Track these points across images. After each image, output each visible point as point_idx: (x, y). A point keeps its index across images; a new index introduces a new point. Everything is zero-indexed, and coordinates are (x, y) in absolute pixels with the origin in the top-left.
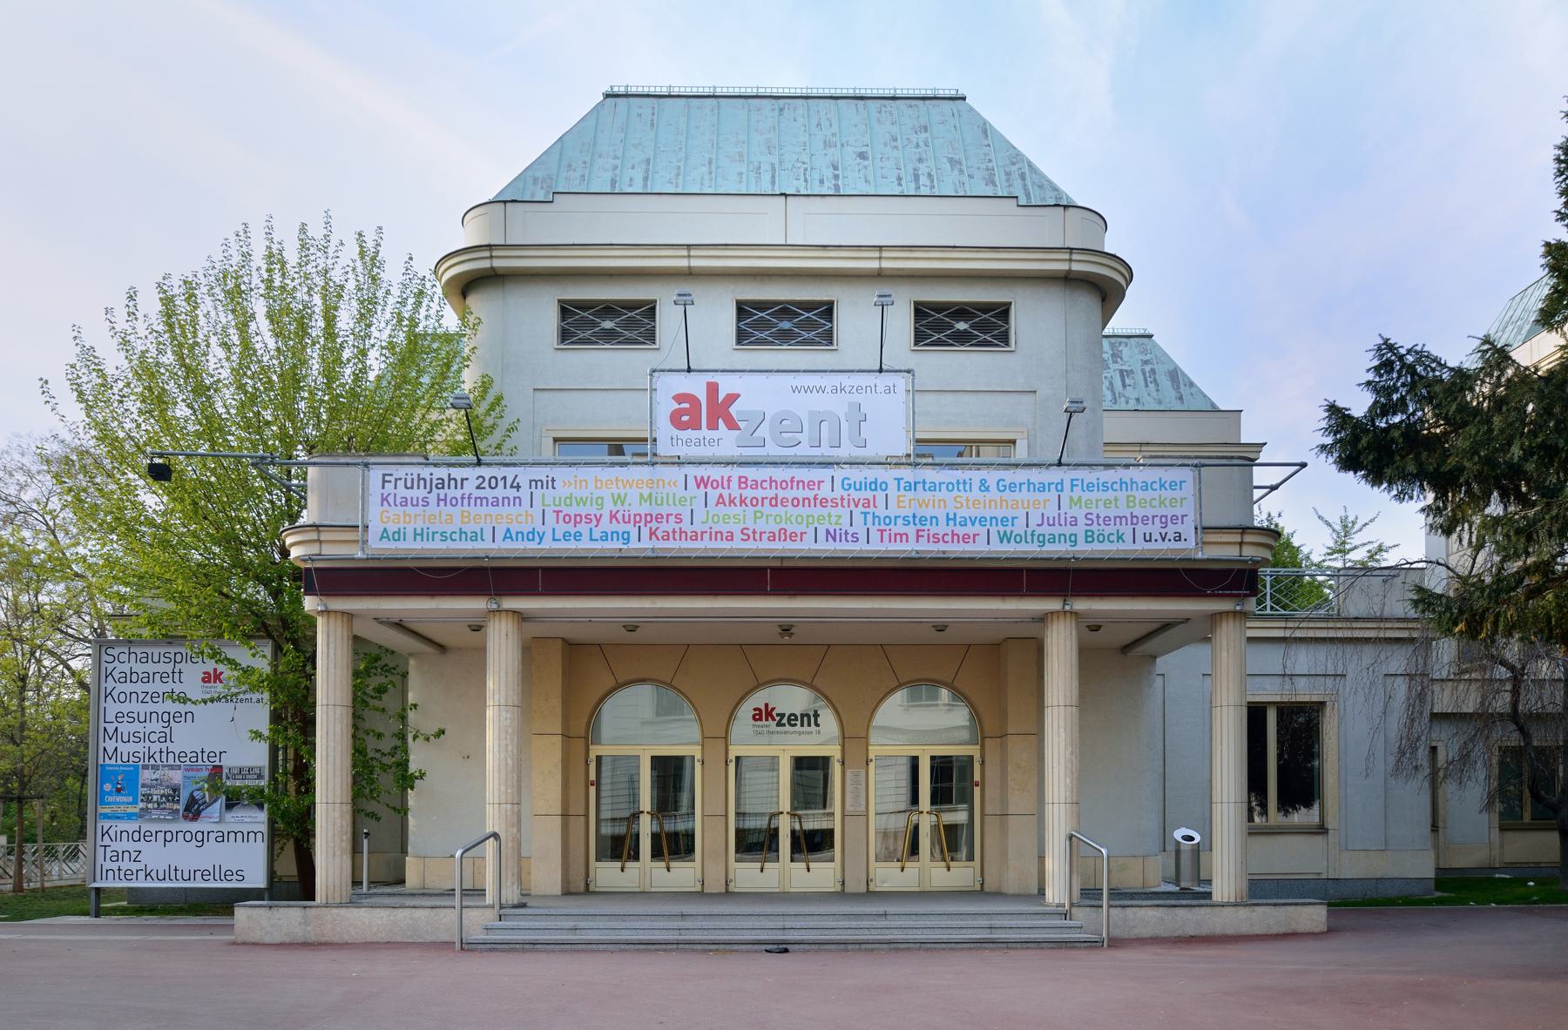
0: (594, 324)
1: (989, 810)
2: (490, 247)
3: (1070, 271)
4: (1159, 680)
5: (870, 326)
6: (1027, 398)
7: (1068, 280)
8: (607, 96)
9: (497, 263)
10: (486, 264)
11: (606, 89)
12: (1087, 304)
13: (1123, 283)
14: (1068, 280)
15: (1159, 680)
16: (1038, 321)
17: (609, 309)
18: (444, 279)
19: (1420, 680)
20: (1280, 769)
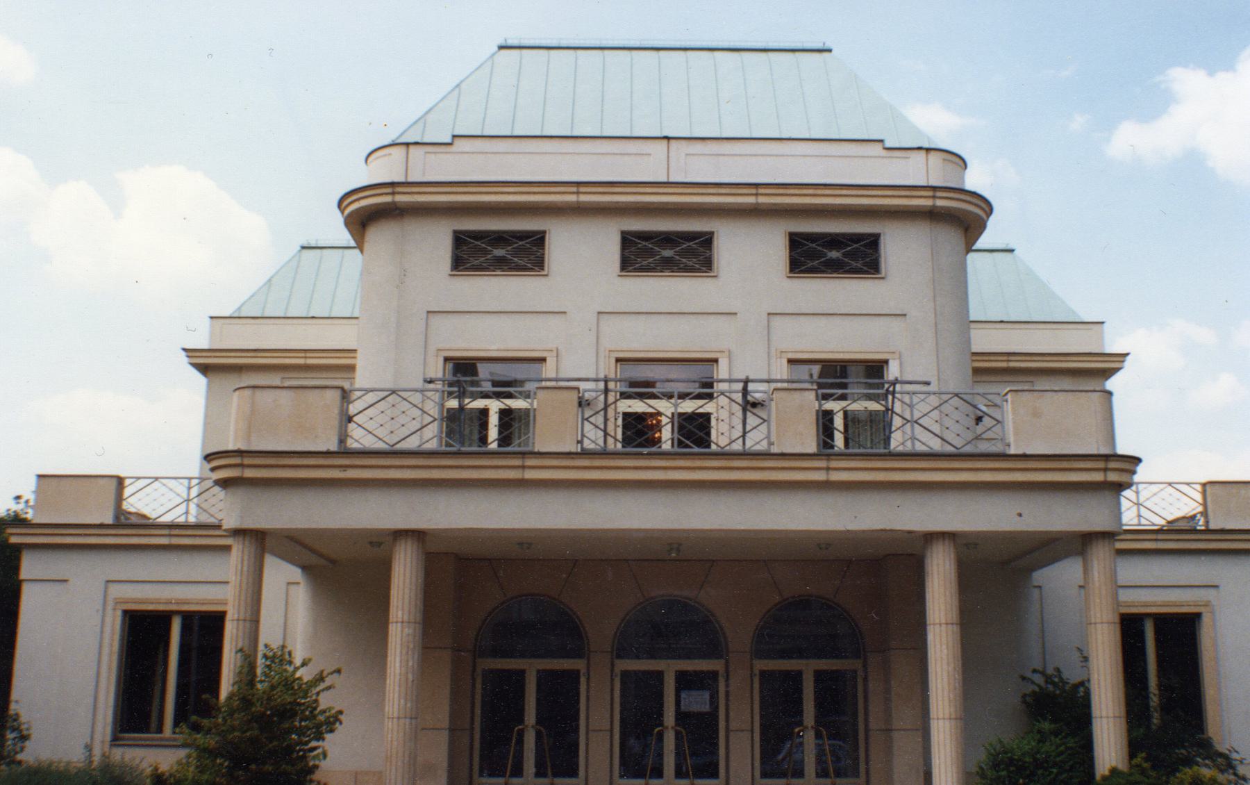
0: (486, 252)
1: (733, 725)
2: (392, 184)
3: (934, 206)
4: (1036, 592)
5: (751, 259)
6: (896, 324)
7: (932, 215)
8: (501, 48)
9: (398, 198)
10: (388, 199)
11: (501, 42)
12: (949, 237)
13: (984, 216)
14: (932, 215)
15: (1036, 592)
16: (902, 248)
17: (500, 238)
18: (347, 212)
19: (352, 384)
20: (799, 701)
